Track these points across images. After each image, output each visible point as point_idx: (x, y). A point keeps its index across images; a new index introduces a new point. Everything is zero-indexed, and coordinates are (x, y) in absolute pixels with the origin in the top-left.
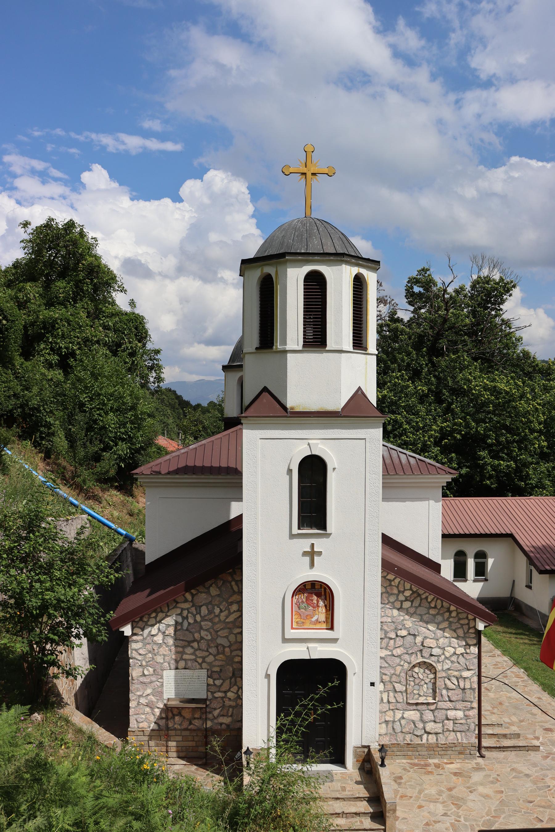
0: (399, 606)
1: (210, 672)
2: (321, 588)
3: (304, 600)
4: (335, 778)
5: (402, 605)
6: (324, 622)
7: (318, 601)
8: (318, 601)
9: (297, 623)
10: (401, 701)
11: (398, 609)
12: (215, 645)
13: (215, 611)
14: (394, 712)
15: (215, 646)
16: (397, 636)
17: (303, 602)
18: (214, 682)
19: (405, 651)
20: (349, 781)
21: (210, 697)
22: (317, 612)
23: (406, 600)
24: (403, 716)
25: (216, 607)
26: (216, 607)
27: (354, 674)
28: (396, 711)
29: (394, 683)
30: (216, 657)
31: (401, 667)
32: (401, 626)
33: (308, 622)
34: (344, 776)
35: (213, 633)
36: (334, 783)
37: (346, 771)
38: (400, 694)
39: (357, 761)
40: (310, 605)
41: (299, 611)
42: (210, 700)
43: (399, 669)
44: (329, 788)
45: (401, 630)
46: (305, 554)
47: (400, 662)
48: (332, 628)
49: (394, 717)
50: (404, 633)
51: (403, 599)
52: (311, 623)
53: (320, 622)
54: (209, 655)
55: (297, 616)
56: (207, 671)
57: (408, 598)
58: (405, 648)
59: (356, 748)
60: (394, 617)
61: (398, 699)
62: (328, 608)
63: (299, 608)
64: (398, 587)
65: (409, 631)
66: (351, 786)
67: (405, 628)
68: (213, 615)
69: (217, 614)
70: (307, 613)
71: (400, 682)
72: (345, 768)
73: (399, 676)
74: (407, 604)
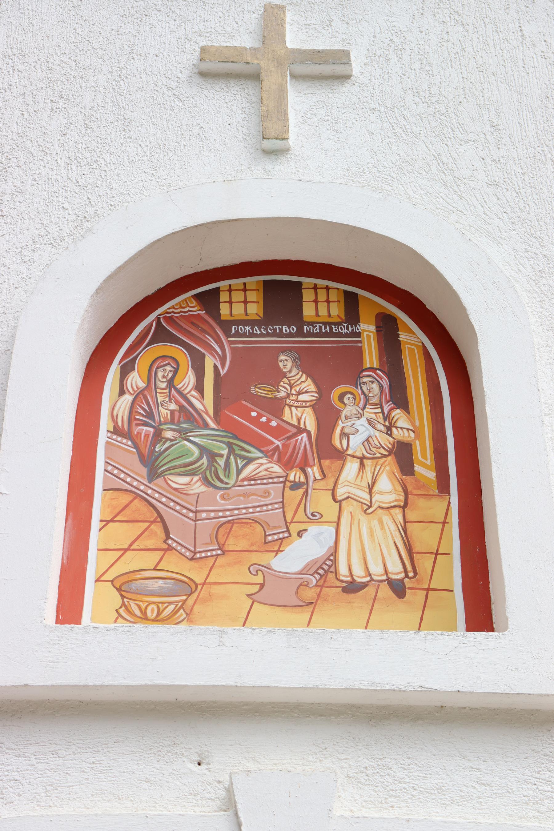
3: (206, 404)
7: (327, 415)
8: (327, 415)
9: (124, 587)
17: (187, 416)
22: (321, 501)
33: (231, 578)
40: (259, 444)
41: (154, 490)
46: (219, 69)
53: (352, 587)
55: (122, 533)
62: (425, 470)
63: (153, 465)
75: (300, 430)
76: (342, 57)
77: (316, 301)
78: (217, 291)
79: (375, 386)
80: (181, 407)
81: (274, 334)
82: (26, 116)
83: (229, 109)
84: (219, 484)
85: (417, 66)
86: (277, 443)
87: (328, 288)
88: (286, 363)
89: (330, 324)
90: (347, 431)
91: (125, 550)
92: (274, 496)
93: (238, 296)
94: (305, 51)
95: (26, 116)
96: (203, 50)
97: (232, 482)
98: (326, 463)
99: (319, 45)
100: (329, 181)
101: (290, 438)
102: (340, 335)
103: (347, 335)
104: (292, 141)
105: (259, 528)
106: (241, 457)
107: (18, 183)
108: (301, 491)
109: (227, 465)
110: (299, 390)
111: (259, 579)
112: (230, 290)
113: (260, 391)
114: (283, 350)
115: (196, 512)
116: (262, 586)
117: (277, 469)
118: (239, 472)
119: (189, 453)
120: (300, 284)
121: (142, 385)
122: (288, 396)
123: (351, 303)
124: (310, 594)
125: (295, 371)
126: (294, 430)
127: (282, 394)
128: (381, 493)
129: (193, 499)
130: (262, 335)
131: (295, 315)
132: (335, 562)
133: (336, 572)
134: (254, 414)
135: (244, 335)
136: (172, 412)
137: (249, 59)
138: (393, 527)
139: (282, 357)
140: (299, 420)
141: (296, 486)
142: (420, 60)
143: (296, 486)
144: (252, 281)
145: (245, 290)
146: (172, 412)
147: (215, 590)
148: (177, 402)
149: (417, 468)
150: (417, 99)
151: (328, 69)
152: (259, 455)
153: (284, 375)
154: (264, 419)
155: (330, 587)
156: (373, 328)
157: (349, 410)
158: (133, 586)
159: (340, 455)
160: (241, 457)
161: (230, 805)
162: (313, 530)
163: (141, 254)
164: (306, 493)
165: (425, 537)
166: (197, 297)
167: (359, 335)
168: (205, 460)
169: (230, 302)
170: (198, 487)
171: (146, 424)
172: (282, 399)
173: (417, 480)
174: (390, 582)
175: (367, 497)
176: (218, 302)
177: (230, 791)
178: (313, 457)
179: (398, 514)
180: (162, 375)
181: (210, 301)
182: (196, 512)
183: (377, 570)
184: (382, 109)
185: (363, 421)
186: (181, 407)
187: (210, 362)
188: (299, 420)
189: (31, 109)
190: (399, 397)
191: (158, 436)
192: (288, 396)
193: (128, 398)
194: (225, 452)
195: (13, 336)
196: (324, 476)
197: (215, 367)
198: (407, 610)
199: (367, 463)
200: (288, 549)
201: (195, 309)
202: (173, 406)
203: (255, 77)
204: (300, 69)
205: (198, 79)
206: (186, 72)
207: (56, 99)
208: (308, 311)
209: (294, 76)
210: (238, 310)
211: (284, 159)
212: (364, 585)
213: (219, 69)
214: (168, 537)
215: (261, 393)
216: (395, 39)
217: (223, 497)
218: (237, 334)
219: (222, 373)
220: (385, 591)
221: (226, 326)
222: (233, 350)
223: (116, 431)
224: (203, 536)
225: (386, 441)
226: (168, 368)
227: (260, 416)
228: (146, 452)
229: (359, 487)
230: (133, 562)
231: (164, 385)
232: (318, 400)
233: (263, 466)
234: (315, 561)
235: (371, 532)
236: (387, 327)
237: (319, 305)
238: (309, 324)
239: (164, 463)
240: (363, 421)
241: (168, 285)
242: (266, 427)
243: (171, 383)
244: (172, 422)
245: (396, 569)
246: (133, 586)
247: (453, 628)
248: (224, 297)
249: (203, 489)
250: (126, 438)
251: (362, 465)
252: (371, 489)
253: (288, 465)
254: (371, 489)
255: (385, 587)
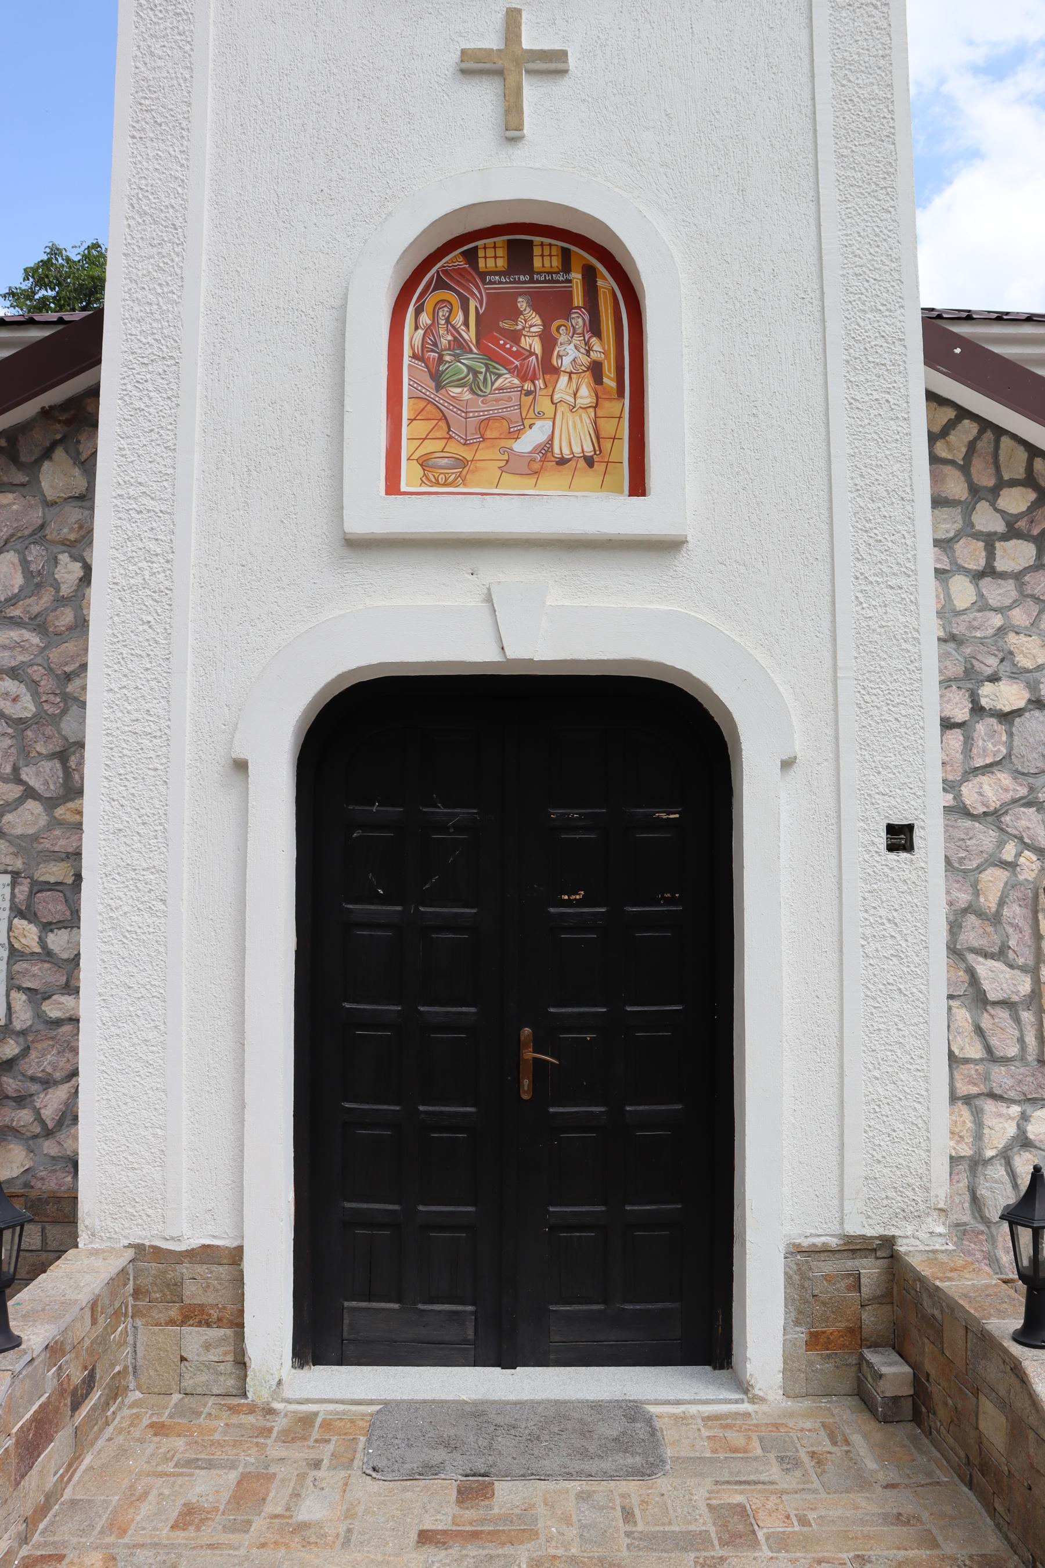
0: (978, 562)
1: (23, 889)
2: (566, 268)
3: (470, 335)
4: (675, 1445)
5: (991, 555)
6: (590, 462)
7: (549, 342)
8: (549, 342)
9: (424, 463)
10: (1013, 1051)
11: (978, 576)
12: (55, 745)
13: (61, 573)
14: (978, 1116)
15: (52, 756)
16: (978, 710)
17: (459, 344)
18: (42, 942)
19: (1023, 791)
20: (774, 1472)
21: (23, 1017)
22: (544, 404)
23: (1012, 532)
24: (1022, 1132)
25: (64, 558)
26: (64, 558)
27: (787, 764)
28: (989, 1106)
29: (971, 957)
30: (59, 812)
31: (1003, 875)
32: (993, 661)
33: (489, 456)
34: (736, 1438)
35: (47, 684)
36: (662, 1483)
37: (746, 1407)
38: (1003, 1014)
39: (814, 1340)
40: (505, 364)
41: (439, 398)
42: (23, 1033)
43: (994, 880)
44: (628, 1515)
45: (994, 679)
46: (474, 66)
47: (1001, 845)
48: (638, 486)
49: (978, 1136)
50: (1008, 695)
51: (998, 526)
52: (510, 465)
53: (562, 462)
54: (21, 801)
55: (422, 427)
56: (14, 884)
57: (1022, 524)
58: (1018, 774)
59: (803, 1256)
60: (958, 613)
61: (994, 1041)
62: (610, 382)
63: (438, 379)
64: (965, 469)
65: (1033, 687)
66: (791, 1504)
67: (1017, 674)
68: (47, 597)
69: (65, 590)
70: (481, 407)
71: (1001, 954)
72: (744, 1388)
73: (995, 920)
74: (1016, 555)
75: (532, 354)
76: (561, 55)
77: (542, 256)
78: (476, 248)
79: (580, 320)
80: (455, 337)
81: (515, 282)
82: (342, 114)
83: (482, 99)
84: (480, 393)
85: (615, 61)
86: (517, 363)
87: (550, 245)
88: (522, 303)
89: (551, 273)
90: (561, 353)
91: (424, 439)
92: (515, 402)
93: (490, 253)
94: (536, 51)
95: (342, 114)
96: (464, 52)
97: (488, 391)
98: (547, 377)
99: (546, 47)
100: (550, 170)
101: (524, 359)
102: (558, 282)
103: (562, 282)
104: (526, 131)
105: (505, 423)
106: (494, 373)
107: (340, 171)
108: (531, 397)
109: (485, 379)
110: (532, 322)
111: (506, 457)
112: (485, 248)
113: (505, 325)
114: (521, 294)
115: (466, 413)
116: (507, 461)
117: (516, 381)
118: (493, 384)
119: (461, 371)
120: (532, 241)
121: (429, 322)
122: (524, 328)
123: (566, 254)
124: (536, 466)
125: (528, 310)
126: (527, 354)
127: (520, 327)
128: (581, 398)
129: (464, 404)
130: (506, 283)
131: (529, 269)
132: (552, 445)
133: (552, 452)
134: (502, 342)
135: (495, 283)
136: (449, 341)
137: (495, 60)
138: (588, 421)
139: (520, 300)
140: (531, 346)
141: (528, 393)
142: (618, 55)
143: (528, 393)
144: (500, 240)
145: (495, 247)
146: (449, 341)
147: (480, 464)
148: (452, 335)
149: (605, 380)
150: (615, 91)
151: (552, 64)
152: (505, 371)
153: (521, 313)
154: (508, 346)
155: (548, 460)
156: (580, 276)
157: (562, 338)
158: (430, 463)
159: (556, 371)
160: (494, 373)
161: (489, 599)
162: (539, 423)
163: (424, 231)
164: (535, 398)
165: (607, 427)
166: (463, 253)
167: (570, 281)
168: (471, 376)
169: (485, 257)
170: (467, 396)
171: (433, 351)
172: (520, 330)
173: (604, 389)
174: (585, 458)
175: (573, 400)
176: (477, 257)
177: (489, 589)
178: (539, 373)
179: (591, 411)
180: (443, 313)
181: (471, 256)
182: (466, 413)
183: (577, 450)
184: (590, 99)
185: (572, 346)
186: (455, 337)
187: (473, 304)
188: (531, 346)
189: (344, 108)
190: (595, 328)
191: (441, 360)
192: (524, 328)
193: (420, 332)
194: (483, 370)
195: (346, 295)
196: (546, 386)
197: (476, 307)
198: (592, 478)
199: (574, 376)
200: (523, 437)
201: (461, 263)
202: (450, 338)
203: (500, 73)
204: (531, 66)
205: (459, 73)
206: (451, 69)
207: (360, 98)
208: (537, 263)
209: (528, 72)
210: (491, 263)
211: (520, 145)
212: (569, 460)
213: (474, 66)
214: (449, 430)
215: (506, 326)
216: (601, 36)
217: (482, 402)
218: (490, 283)
219: (481, 312)
220: (582, 463)
221: (483, 275)
222: (487, 294)
223: (414, 356)
224: (471, 429)
225: (585, 360)
226: (446, 309)
227: (505, 343)
228: (434, 371)
229: (568, 394)
230: (429, 447)
231: (443, 322)
232: (543, 330)
233: (508, 379)
234: (540, 445)
235: (574, 423)
236: (590, 275)
237: (546, 259)
238: (538, 273)
239: (445, 379)
240: (572, 346)
241: (444, 245)
242: (509, 351)
243: (448, 321)
244: (449, 349)
245: (589, 449)
246: (430, 463)
247: (621, 492)
248: (481, 253)
249: (470, 396)
250: (518, 1053)
251: (570, 378)
252: (575, 395)
253: (523, 379)
254: (575, 395)
255: (582, 461)
